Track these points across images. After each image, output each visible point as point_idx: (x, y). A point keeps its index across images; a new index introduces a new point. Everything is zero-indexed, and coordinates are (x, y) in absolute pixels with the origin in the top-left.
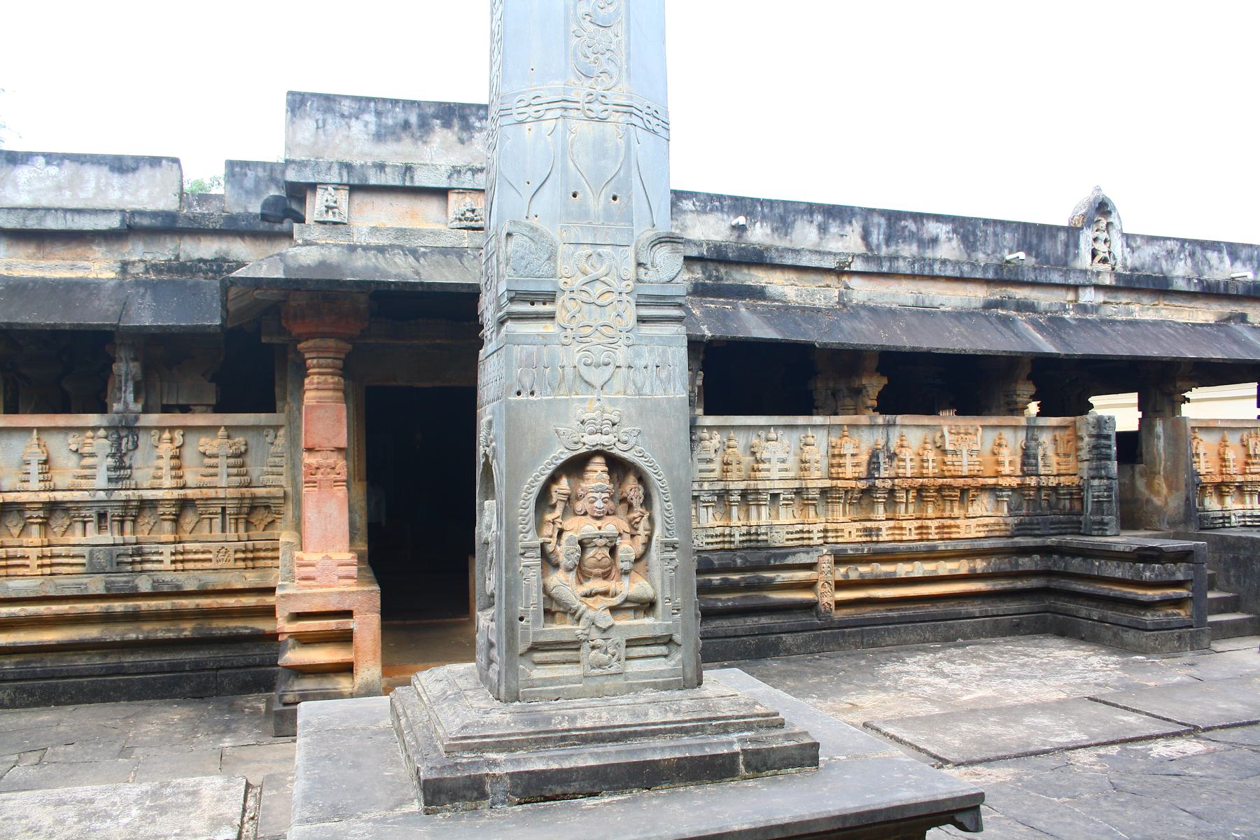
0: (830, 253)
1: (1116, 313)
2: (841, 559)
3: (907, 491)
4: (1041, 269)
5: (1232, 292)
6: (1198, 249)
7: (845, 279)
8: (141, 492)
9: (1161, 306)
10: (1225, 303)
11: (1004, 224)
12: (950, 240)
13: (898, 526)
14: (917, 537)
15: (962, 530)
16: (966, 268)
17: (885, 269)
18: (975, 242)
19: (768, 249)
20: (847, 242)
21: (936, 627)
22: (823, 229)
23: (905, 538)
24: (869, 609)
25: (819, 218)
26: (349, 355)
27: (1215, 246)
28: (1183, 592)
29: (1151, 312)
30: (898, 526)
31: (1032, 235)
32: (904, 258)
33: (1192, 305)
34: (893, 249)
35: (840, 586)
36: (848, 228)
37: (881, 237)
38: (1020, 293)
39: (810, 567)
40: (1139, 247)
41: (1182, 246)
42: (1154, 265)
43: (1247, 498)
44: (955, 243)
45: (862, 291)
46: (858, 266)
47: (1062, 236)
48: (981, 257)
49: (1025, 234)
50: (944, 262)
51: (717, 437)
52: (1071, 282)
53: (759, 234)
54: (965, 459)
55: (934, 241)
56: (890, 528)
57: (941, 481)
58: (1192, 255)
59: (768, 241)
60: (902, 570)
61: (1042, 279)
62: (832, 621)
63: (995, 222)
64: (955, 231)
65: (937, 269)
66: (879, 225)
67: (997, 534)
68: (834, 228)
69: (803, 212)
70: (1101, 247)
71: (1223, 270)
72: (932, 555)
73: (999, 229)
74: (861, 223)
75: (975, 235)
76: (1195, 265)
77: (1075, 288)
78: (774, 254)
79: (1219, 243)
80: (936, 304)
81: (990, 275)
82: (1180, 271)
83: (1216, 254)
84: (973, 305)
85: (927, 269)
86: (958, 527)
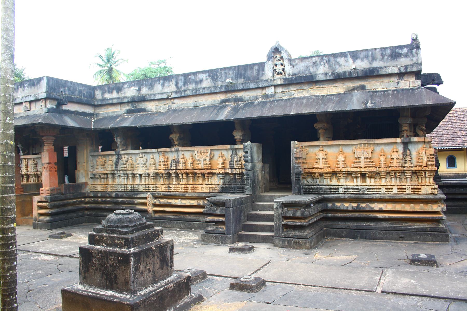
0: (165, 93)
1: (284, 96)
2: (156, 197)
3: (182, 174)
4: (245, 83)
5: (354, 75)
6: (332, 59)
7: (172, 100)
8: (195, 170)
9: (315, 88)
10: (355, 81)
11: (229, 68)
12: (207, 79)
13: (178, 187)
14: (183, 191)
15: (200, 189)
16: (213, 89)
17: (183, 95)
18: (217, 78)
19: (146, 95)
20: (171, 88)
21: (184, 223)
22: (163, 85)
23: (179, 191)
24: (166, 214)
25: (162, 82)
26: (55, 140)
27: (343, 55)
28: (221, 219)
29: (304, 92)
30: (178, 187)
31: (241, 71)
32: (189, 90)
33: (334, 85)
34: (186, 87)
35: (155, 205)
36: (171, 83)
37: (182, 84)
38: (239, 95)
39: (146, 198)
40: (297, 64)
41: (322, 58)
42: (305, 71)
43: (355, 180)
44: (209, 80)
45: (178, 104)
46: (174, 96)
47: (256, 67)
48: (220, 83)
49: (238, 70)
50: (204, 88)
51: (126, 157)
52: (260, 86)
53: (145, 91)
54: (202, 162)
55: (201, 81)
56: (192, 188)
57: (193, 170)
58: (328, 62)
59: (147, 93)
60: (173, 202)
61: (246, 87)
62: (152, 217)
63: (225, 68)
64: (209, 76)
65: (202, 92)
66: (181, 80)
67: (216, 191)
68: (166, 84)
69: (157, 81)
70: (279, 68)
71: (349, 65)
72: (183, 197)
73: (227, 71)
74: (175, 80)
75: (217, 75)
76: (330, 66)
77: (263, 88)
78: (148, 97)
79: (345, 53)
80: (201, 105)
81: (223, 90)
82: (321, 71)
83: (343, 59)
84: (216, 102)
85: (198, 92)
86: (198, 188)
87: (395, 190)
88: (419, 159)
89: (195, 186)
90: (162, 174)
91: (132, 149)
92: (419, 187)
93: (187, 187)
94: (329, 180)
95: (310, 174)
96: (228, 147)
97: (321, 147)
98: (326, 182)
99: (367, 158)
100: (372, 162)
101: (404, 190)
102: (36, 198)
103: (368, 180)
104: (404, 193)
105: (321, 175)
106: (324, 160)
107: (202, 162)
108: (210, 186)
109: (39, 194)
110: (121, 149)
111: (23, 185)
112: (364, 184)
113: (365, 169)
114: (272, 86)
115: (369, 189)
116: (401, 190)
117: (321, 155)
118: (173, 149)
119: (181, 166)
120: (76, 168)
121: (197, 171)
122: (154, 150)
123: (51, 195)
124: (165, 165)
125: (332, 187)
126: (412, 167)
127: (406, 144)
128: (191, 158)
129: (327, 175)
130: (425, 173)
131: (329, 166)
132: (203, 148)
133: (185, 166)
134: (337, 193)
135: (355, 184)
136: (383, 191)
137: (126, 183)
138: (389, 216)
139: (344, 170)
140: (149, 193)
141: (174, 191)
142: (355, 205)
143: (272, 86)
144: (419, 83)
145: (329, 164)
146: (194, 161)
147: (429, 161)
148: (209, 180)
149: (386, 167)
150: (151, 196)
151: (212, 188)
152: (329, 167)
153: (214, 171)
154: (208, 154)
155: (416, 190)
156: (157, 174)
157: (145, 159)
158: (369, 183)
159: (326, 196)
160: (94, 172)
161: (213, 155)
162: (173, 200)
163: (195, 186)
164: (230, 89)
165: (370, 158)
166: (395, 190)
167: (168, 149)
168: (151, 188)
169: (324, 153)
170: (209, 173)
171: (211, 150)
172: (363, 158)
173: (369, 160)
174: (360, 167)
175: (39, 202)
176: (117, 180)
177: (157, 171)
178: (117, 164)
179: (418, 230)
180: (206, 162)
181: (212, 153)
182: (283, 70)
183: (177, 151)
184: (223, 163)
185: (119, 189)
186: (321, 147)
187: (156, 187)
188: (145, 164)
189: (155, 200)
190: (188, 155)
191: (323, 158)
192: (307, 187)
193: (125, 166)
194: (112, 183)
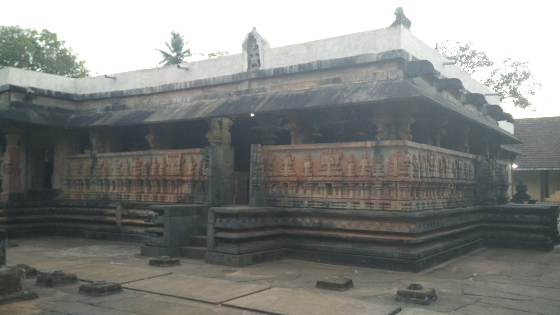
30: (148, 196)
35: (124, 216)
87: (362, 206)
90: (135, 181)
91: (111, 152)
92: (388, 202)
94: (294, 191)
95: (275, 183)
96: (198, 150)
99: (334, 165)
105: (286, 184)
106: (290, 167)
112: (329, 197)
113: (330, 179)
114: (245, 80)
115: (335, 203)
116: (369, 205)
118: (146, 152)
119: (153, 173)
120: (52, 174)
121: (167, 178)
122: (128, 153)
126: (383, 177)
127: (377, 149)
129: (292, 185)
130: (396, 184)
131: (295, 174)
135: (321, 196)
136: (349, 206)
137: (100, 191)
138: (352, 237)
140: (118, 203)
142: (317, 221)
143: (245, 80)
144: (401, 73)
145: (295, 172)
147: (401, 170)
149: (355, 177)
150: (120, 206)
154: (179, 159)
158: (336, 196)
159: (287, 209)
161: (183, 160)
163: (165, 195)
166: (362, 206)
167: (141, 153)
169: (290, 159)
172: (329, 165)
173: (336, 168)
176: (92, 187)
178: (92, 168)
183: (150, 155)
184: (193, 169)
192: (272, 198)
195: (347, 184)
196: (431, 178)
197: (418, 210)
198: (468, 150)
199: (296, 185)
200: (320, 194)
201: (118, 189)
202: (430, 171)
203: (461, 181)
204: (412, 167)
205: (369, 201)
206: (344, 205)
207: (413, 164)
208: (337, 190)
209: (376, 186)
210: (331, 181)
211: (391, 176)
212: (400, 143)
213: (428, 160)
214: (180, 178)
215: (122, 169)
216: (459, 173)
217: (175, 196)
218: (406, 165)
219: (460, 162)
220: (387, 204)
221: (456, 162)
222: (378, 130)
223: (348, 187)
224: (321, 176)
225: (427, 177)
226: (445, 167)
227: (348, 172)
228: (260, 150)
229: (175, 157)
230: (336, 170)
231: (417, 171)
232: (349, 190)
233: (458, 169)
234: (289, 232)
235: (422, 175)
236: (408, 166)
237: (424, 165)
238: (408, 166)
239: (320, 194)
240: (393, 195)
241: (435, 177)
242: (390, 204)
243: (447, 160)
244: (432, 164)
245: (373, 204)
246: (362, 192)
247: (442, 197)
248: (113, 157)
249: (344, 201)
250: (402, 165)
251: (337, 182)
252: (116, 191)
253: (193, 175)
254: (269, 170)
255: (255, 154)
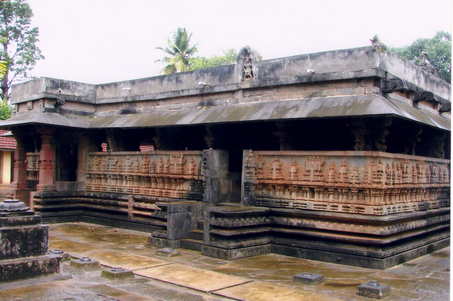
2: (137, 200)
7: (158, 102)
14: (159, 195)
15: (172, 194)
39: (127, 201)
51: (116, 158)
54: (175, 167)
86: (171, 193)
87: (340, 209)
88: (365, 176)
89: (169, 191)
90: (143, 177)
92: (363, 206)
93: (162, 192)
96: (198, 152)
97: (276, 157)
98: (279, 194)
100: (321, 176)
101: (348, 209)
102: (33, 194)
103: (316, 195)
104: (349, 212)
105: (274, 186)
106: (278, 171)
107: (175, 167)
108: (181, 192)
109: (36, 190)
110: (112, 150)
111: (28, 181)
112: (312, 199)
116: (346, 209)
117: (275, 166)
121: (171, 176)
123: (44, 192)
124: (146, 168)
125: (283, 201)
126: (359, 184)
128: (167, 162)
129: (279, 188)
130: (370, 191)
131: (282, 177)
132: (177, 153)
133: (155, 170)
134: (287, 207)
136: (329, 208)
139: (294, 183)
140: (130, 196)
141: (151, 195)
145: (282, 176)
146: (170, 165)
147: (375, 178)
148: (181, 185)
149: (335, 183)
151: (182, 194)
152: (283, 179)
153: (185, 177)
154: (180, 160)
155: (360, 210)
156: (140, 177)
157: (131, 160)
158: (319, 198)
160: (91, 172)
162: (149, 204)
163: (169, 191)
164: (206, 91)
165: (320, 171)
168: (134, 191)
170: (180, 179)
171: (184, 155)
172: (312, 171)
173: (318, 174)
174: (309, 181)
175: (35, 197)
177: (139, 174)
179: (144, 223)
180: (179, 167)
181: (185, 158)
182: (252, 73)
184: (193, 169)
185: (109, 190)
186: (276, 157)
187: (138, 190)
188: (131, 166)
189: (135, 203)
190: (165, 159)
191: (277, 169)
193: (115, 167)
194: (104, 184)
195: (328, 189)
196: (403, 184)
197: (389, 214)
198: (443, 155)
199: (283, 188)
200: (303, 196)
201: (130, 184)
202: (403, 177)
203: (433, 185)
204: (384, 175)
205: (346, 205)
206: (324, 207)
207: (386, 173)
208: (319, 193)
209: (352, 191)
210: (314, 185)
211: (365, 183)
212: (375, 154)
213: (402, 168)
214: (181, 176)
215: (133, 167)
216: (433, 177)
217: (177, 192)
218: (379, 174)
219: (434, 168)
220: (361, 208)
221: (430, 167)
222: (355, 141)
223: (329, 191)
224: (305, 181)
225: (399, 184)
226: (419, 173)
227: (328, 178)
228: (251, 155)
229: (178, 157)
230: (318, 176)
231: (390, 178)
232: (330, 194)
233: (432, 174)
234: (276, 230)
235: (393, 182)
236: (381, 175)
237: (396, 173)
238: (381, 175)
239: (303, 196)
240: (367, 200)
241: (407, 183)
242: (364, 209)
243: (421, 166)
244: (405, 171)
245: (349, 207)
246: (340, 196)
247: (415, 200)
248: (126, 155)
249: (325, 203)
250: (376, 174)
251: (319, 187)
252: (128, 185)
253: (193, 174)
254: (259, 173)
255: (247, 158)
